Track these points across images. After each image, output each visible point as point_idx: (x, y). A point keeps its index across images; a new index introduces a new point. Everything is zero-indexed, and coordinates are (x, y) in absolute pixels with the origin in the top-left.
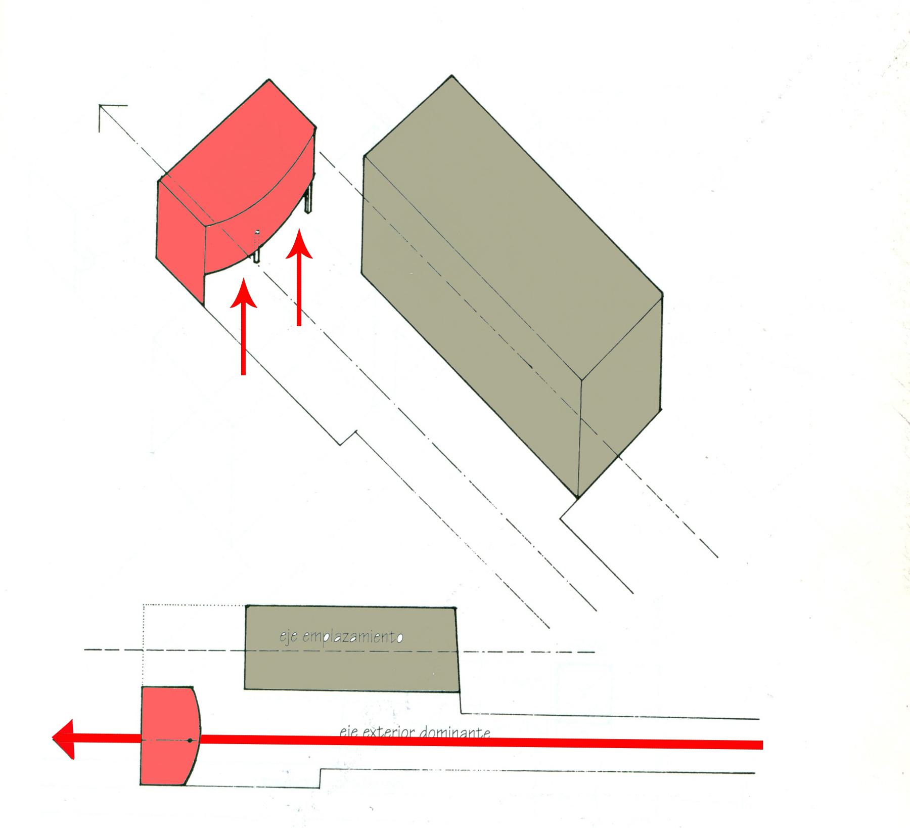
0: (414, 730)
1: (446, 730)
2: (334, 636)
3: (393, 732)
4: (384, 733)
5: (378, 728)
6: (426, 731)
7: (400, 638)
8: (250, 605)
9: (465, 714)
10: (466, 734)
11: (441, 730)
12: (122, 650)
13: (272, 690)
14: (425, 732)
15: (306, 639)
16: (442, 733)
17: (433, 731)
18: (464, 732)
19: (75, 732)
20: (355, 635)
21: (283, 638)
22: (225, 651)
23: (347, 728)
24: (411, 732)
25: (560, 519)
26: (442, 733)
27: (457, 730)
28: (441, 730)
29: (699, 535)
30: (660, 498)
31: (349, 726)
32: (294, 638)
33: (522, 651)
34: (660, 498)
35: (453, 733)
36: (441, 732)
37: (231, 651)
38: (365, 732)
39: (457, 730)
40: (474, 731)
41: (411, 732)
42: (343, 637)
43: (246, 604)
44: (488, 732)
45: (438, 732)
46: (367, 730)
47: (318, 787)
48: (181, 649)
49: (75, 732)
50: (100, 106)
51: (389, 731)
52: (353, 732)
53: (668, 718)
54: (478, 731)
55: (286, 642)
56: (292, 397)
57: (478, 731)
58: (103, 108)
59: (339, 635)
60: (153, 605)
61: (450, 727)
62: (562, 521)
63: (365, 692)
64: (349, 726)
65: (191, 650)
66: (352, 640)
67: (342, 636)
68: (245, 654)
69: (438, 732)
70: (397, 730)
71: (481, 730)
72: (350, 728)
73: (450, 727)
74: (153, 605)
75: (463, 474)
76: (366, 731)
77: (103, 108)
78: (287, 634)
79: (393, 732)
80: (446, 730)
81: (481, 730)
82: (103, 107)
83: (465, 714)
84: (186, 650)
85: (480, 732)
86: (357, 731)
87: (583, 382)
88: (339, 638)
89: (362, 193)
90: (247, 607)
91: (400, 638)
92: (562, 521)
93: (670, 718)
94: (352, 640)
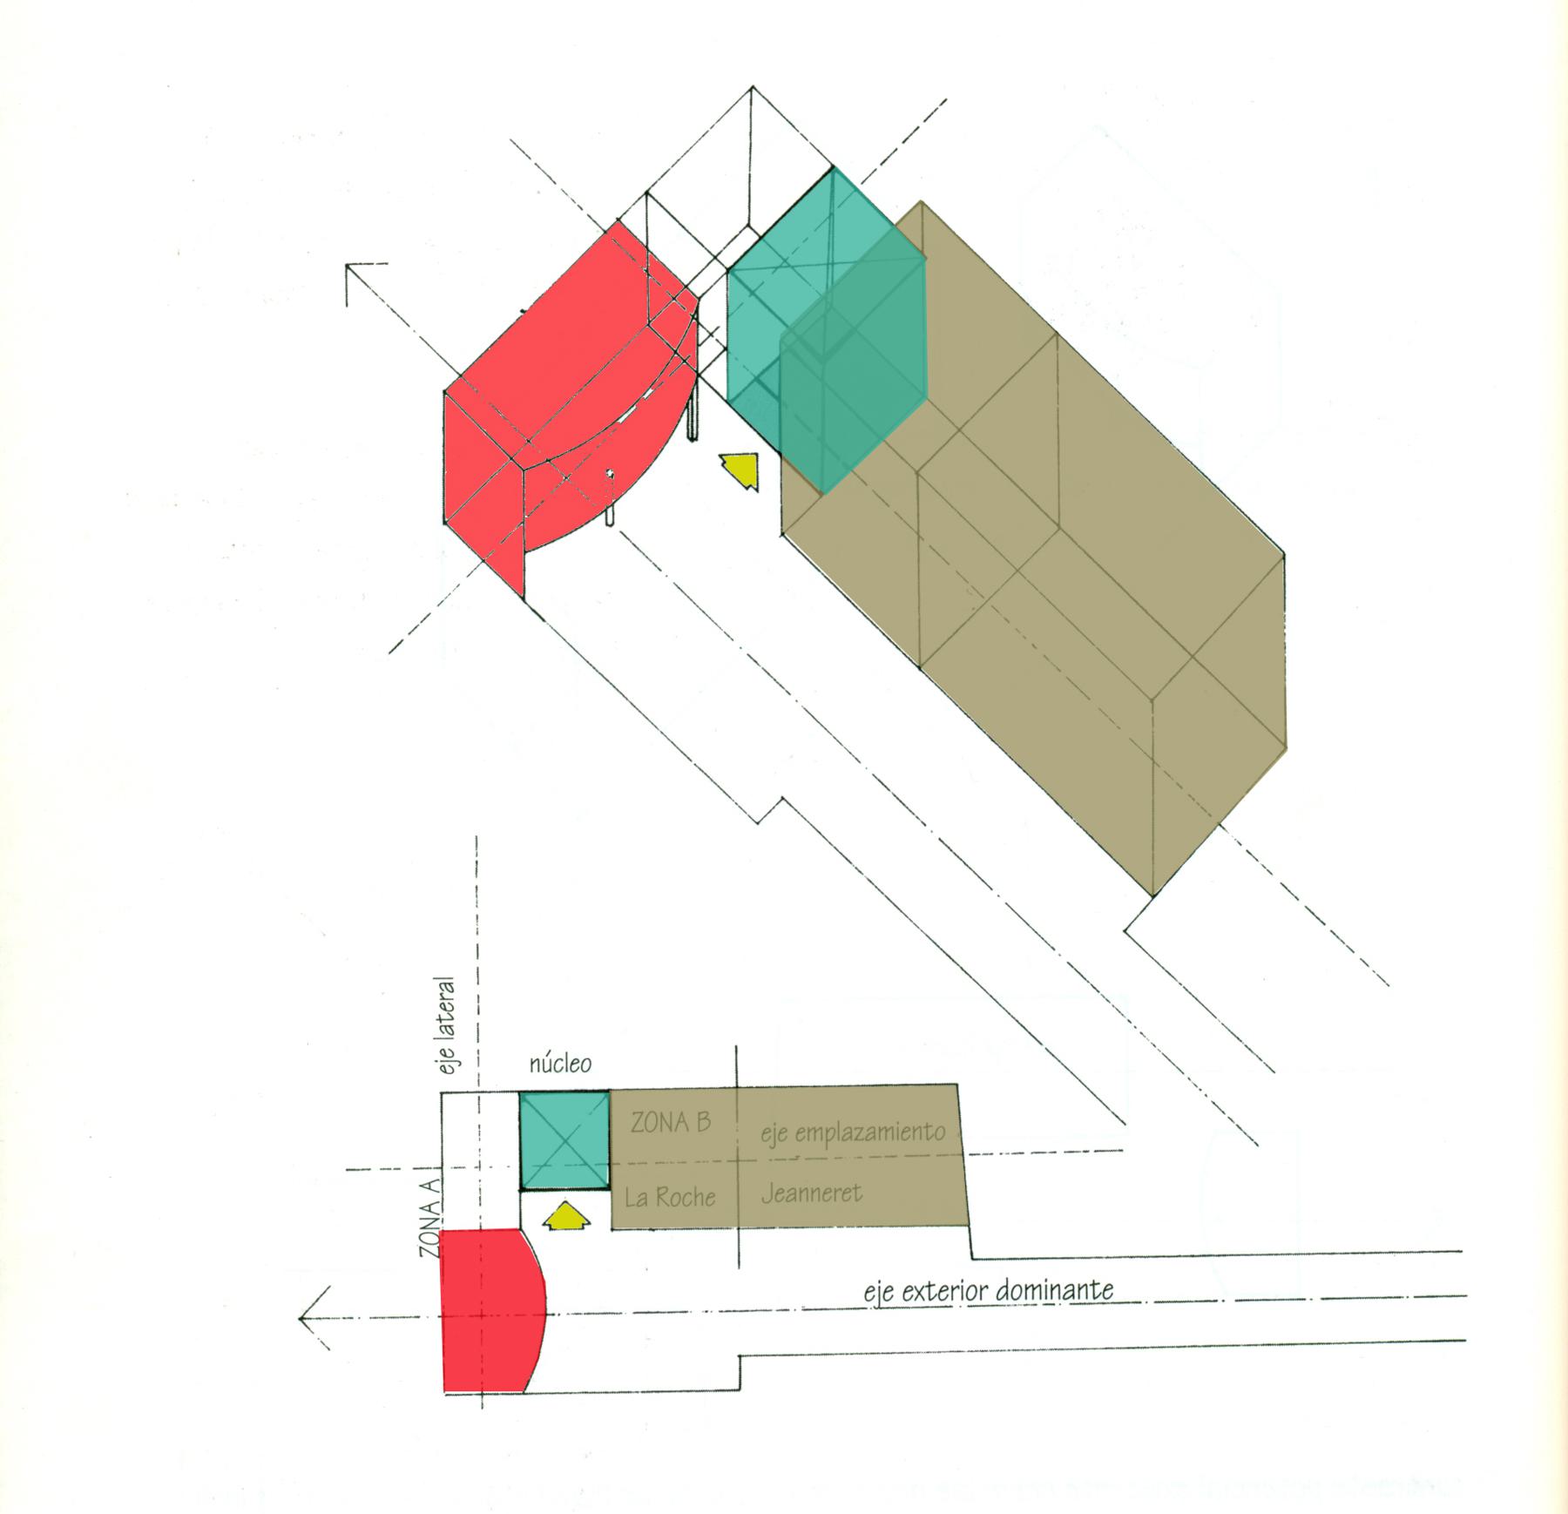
0: (987, 1287)
1: (1040, 1285)
3: (953, 1289)
4: (1102, 1291)
5: (927, 1284)
6: (1007, 1287)
11: (1032, 1285)
18: (1071, 1288)
24: (981, 1289)
25: (442, 1094)
26: (815, 1132)
27: (818, 1189)
28: (1032, 1285)
29: (922, 126)
30: (915, 130)
33: (906, 143)
34: (915, 130)
36: (1031, 1288)
41: (981, 1289)
43: (500, 1404)
44: (890, 1289)
46: (909, 1289)
48: (596, 1391)
53: (1191, 1258)
54: (927, 1127)
57: (927, 1127)
58: (529, 1103)
62: (442, 1098)
64: (879, 1282)
70: (958, 1287)
71: (934, 1285)
77: (529, 1103)
80: (1040, 1285)
81: (934, 1285)
85: (442, 1018)
92: (442, 1098)
93: (902, 455)
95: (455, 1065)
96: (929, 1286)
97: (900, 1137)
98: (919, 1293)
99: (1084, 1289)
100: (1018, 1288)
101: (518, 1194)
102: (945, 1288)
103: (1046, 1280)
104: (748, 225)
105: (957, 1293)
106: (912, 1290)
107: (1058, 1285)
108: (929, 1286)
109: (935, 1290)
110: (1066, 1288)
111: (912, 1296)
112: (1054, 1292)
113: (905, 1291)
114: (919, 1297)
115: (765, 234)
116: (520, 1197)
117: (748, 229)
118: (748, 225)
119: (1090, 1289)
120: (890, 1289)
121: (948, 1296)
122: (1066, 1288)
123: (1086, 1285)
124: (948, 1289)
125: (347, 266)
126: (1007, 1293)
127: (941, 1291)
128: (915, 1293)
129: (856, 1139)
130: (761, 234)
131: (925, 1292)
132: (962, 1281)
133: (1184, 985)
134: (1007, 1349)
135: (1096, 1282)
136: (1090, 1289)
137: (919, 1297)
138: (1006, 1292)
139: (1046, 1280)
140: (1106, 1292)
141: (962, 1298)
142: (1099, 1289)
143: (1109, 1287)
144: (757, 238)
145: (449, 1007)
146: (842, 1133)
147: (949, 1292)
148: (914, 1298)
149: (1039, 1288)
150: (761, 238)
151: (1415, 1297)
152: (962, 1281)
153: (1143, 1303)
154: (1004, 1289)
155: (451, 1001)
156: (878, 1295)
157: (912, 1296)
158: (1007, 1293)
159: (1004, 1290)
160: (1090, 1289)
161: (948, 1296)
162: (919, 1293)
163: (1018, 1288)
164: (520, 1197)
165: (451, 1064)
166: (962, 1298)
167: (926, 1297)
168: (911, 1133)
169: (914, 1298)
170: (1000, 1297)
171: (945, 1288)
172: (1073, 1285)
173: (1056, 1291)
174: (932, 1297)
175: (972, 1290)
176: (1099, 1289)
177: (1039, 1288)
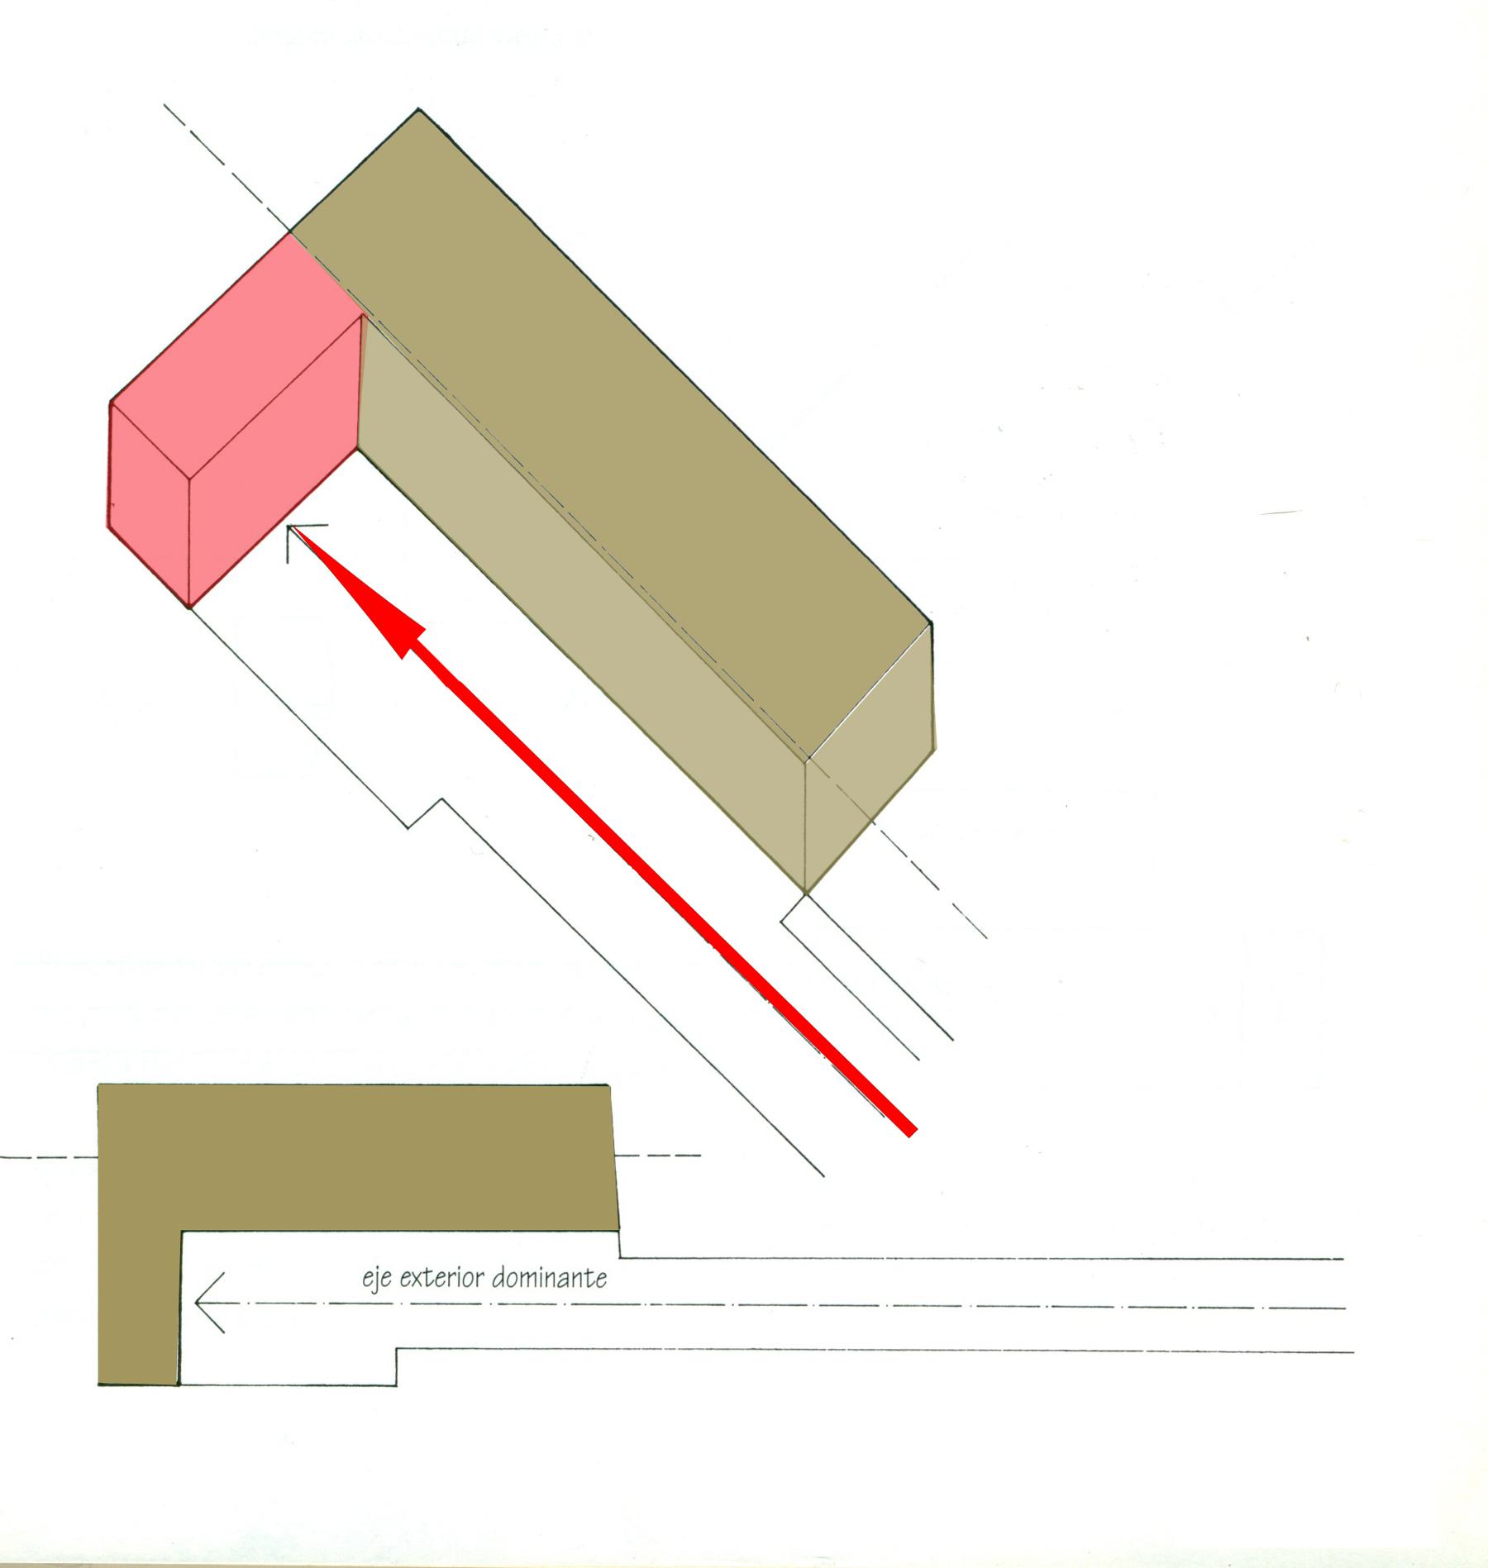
0: (483, 1273)
1: (535, 1273)
3: (450, 1276)
6: (503, 1274)
9: (785, 926)
10: (567, 1279)
11: (528, 1273)
16: (529, 1277)
17: (513, 1275)
18: (565, 1276)
19: (419, 639)
22: (499, 1304)
24: (478, 1276)
26: (529, 1277)
28: (528, 1273)
31: (378, 1267)
37: (960, 1306)
39: (553, 1273)
41: (478, 1276)
44: (388, 1274)
45: (522, 1276)
49: (419, 639)
50: (197, 1303)
52: (383, 1277)
54: (588, 1273)
56: (1083, 1307)
57: (588, 1273)
64: (378, 1267)
65: (414, 1304)
70: (455, 1273)
72: (379, 1270)
75: (253, 1304)
76: (368, 1275)
79: (450, 1276)
80: (535, 1273)
82: (200, 1301)
83: (785, 926)
86: (606, 1276)
96: (427, 1272)
98: (417, 1279)
99: (578, 1278)
100: (469, 1275)
101: (190, 611)
102: (442, 1275)
103: (541, 1268)
104: (189, 479)
105: (454, 1279)
106: (410, 1275)
107: (553, 1273)
108: (427, 1272)
110: (560, 1276)
111: (409, 1282)
112: (549, 1279)
113: (365, 1277)
115: (293, 228)
116: (194, 612)
117: (190, 476)
118: (189, 479)
121: (372, 1282)
122: (560, 1276)
124: (445, 1275)
126: (503, 1280)
127: (599, 1278)
128: (412, 1279)
130: (290, 228)
131: (422, 1279)
132: (459, 1268)
135: (590, 1271)
136: (584, 1277)
138: (502, 1279)
139: (541, 1268)
140: (438, 1280)
141: (459, 1285)
142: (593, 1278)
144: (287, 231)
147: (446, 1278)
149: (534, 1276)
150: (290, 231)
152: (459, 1268)
153: (1196, 1308)
157: (409, 1282)
158: (503, 1280)
160: (584, 1277)
161: (372, 1282)
162: (417, 1279)
163: (469, 1275)
164: (194, 612)
166: (459, 1285)
167: (424, 1283)
170: (496, 1283)
171: (442, 1275)
172: (567, 1273)
173: (550, 1279)
174: (590, 1284)
175: (511, 1282)
176: (593, 1278)
177: (534, 1276)
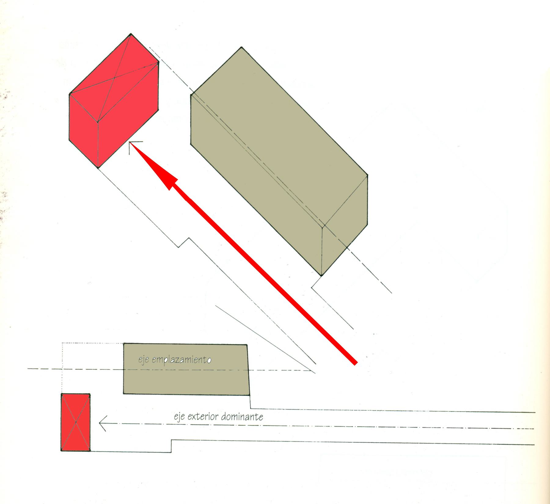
0: (218, 415)
1: (237, 415)
2: (170, 360)
3: (206, 416)
6: (225, 415)
7: (209, 361)
8: (126, 343)
10: (249, 417)
12: (84, 369)
13: (191, 395)
14: (224, 416)
15: (154, 361)
16: (235, 416)
18: (248, 416)
20: (182, 359)
21: (140, 361)
23: (178, 414)
24: (216, 416)
26: (235, 416)
27: (244, 415)
31: (180, 413)
32: (147, 361)
35: (241, 417)
36: (234, 416)
38: (189, 416)
40: (253, 415)
41: (216, 416)
42: (176, 360)
45: (232, 416)
46: (190, 415)
47: (170, 452)
51: (203, 415)
54: (256, 415)
55: (142, 363)
57: (256, 415)
59: (173, 359)
60: (88, 343)
61: (239, 413)
63: (123, 388)
64: (180, 413)
66: (181, 362)
67: (175, 359)
68: (124, 371)
69: (232, 416)
70: (208, 415)
71: (258, 415)
73: (239, 413)
74: (88, 343)
76: (176, 415)
78: (143, 358)
79: (206, 416)
81: (258, 415)
84: (84, 369)
85: (257, 416)
87: (323, 229)
88: (173, 361)
89: (132, 143)
90: (124, 344)
91: (209, 361)
94: (181, 362)
95: (178, 420)
96: (197, 414)
97: (193, 362)
99: (252, 417)
105: (207, 417)
108: (197, 414)
109: (199, 416)
114: (194, 418)
119: (255, 416)
120: (183, 415)
123: (253, 415)
125: (100, 423)
126: (225, 418)
128: (192, 417)
129: (176, 362)
131: (196, 417)
132: (209, 413)
133: (370, 411)
134: (372, 411)
136: (255, 416)
137: (194, 418)
143: (262, 416)
145: (202, 418)
146: (245, 417)
147: (205, 417)
148: (192, 419)
149: (236, 416)
151: (379, 427)
152: (209, 413)
154: (224, 416)
155: (205, 419)
156: (179, 417)
158: (225, 418)
159: (224, 416)
160: (255, 416)
165: (178, 419)
167: (196, 418)
168: (205, 417)
169: (192, 419)
173: (242, 417)
176: (258, 417)
